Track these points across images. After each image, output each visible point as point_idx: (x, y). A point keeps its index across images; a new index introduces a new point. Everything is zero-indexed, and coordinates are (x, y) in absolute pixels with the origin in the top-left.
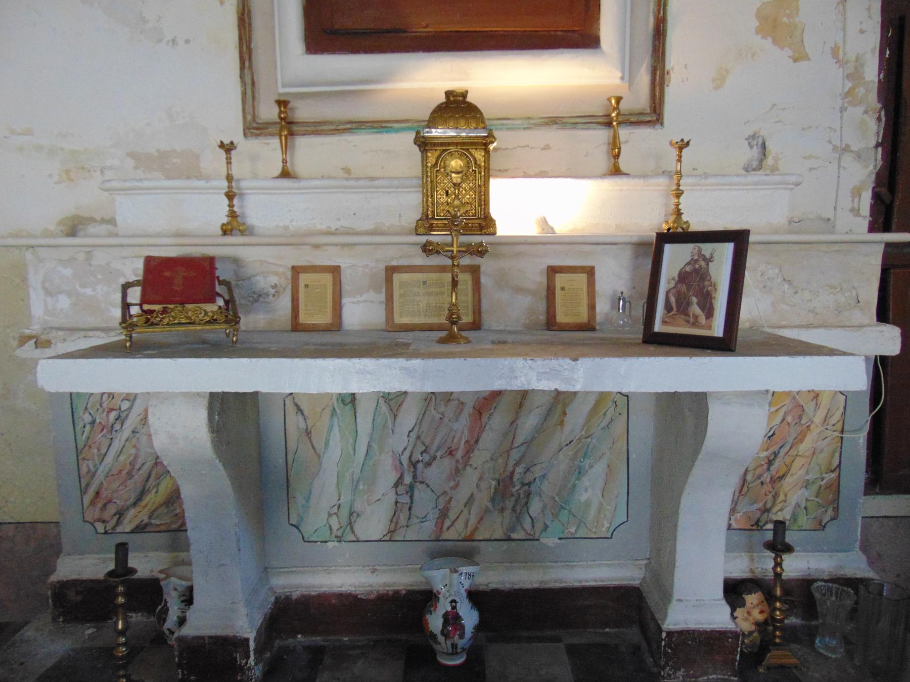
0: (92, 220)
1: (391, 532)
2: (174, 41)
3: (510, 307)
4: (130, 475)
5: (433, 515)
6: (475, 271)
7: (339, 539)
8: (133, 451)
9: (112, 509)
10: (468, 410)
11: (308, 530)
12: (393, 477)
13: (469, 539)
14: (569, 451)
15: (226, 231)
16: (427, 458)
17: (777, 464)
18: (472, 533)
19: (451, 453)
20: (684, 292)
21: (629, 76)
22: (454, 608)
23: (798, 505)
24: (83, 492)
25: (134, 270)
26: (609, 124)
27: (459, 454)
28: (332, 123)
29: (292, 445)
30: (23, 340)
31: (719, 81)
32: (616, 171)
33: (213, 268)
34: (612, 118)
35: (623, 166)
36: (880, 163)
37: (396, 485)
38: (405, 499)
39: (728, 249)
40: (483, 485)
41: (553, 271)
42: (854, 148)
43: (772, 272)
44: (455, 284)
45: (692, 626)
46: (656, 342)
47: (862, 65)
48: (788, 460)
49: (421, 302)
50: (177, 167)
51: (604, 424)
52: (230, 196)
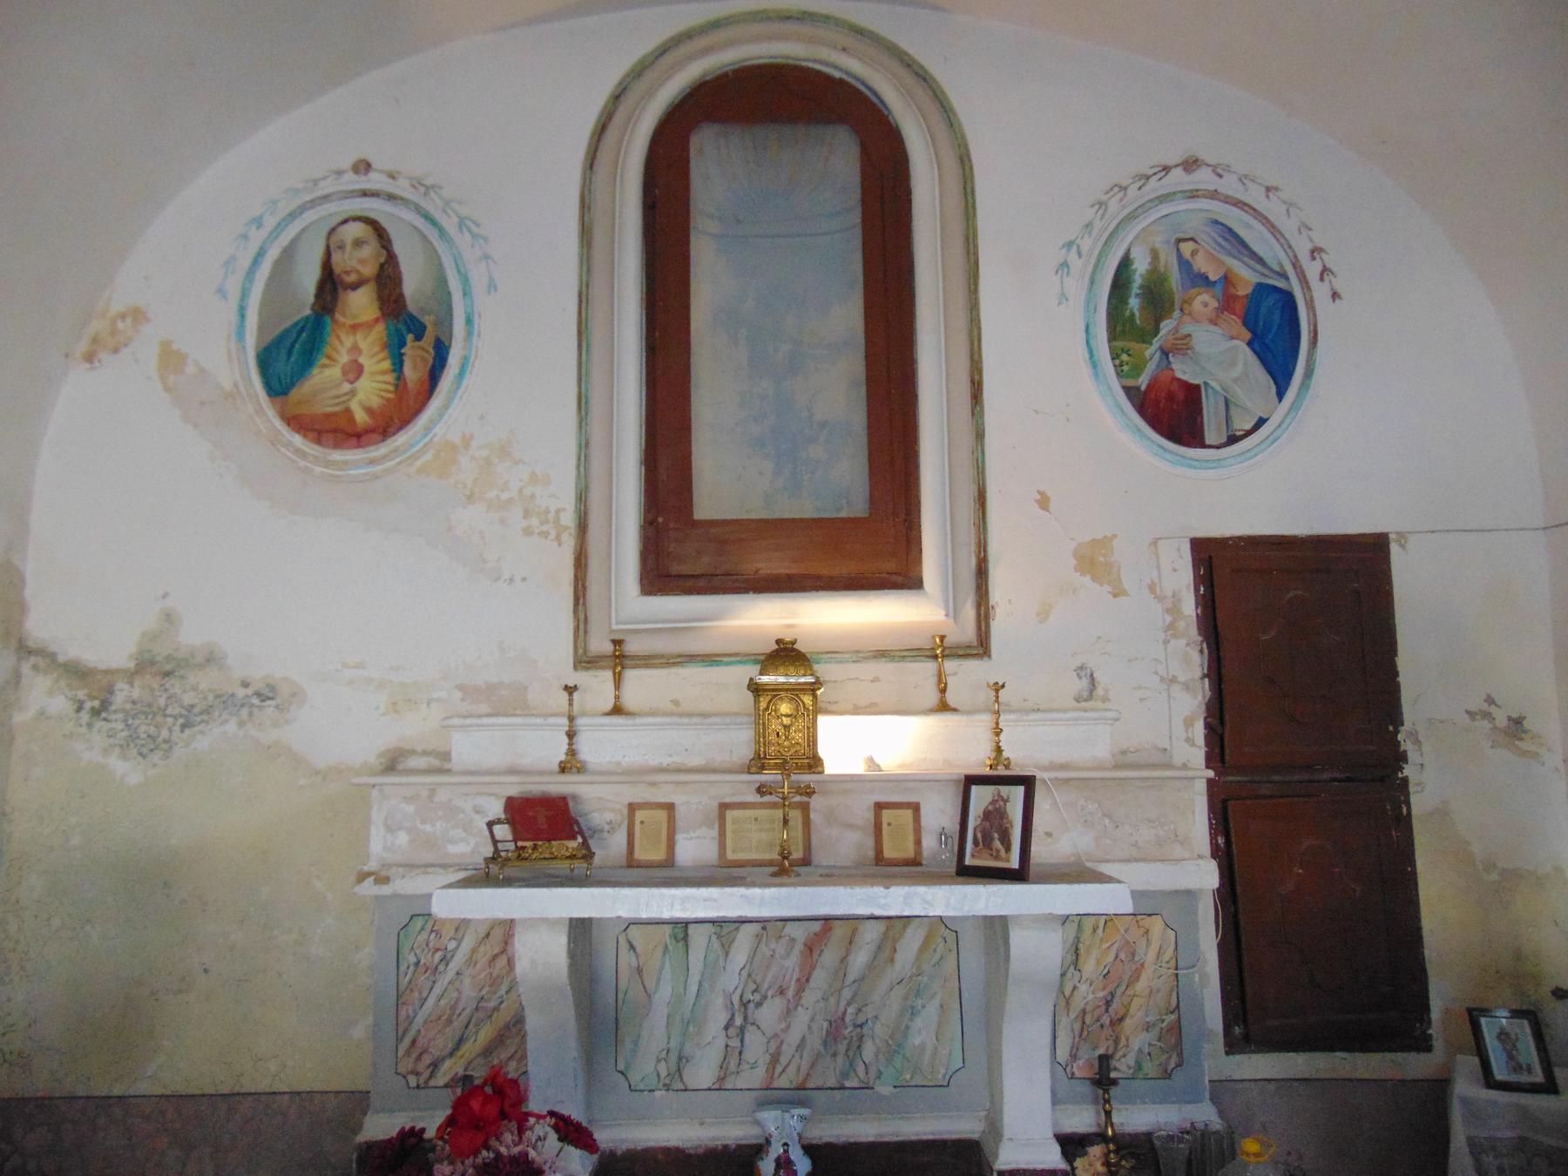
0: (413, 752)
1: (721, 1079)
2: (511, 580)
3: (843, 841)
4: (449, 1022)
5: (764, 1060)
6: (805, 808)
7: (667, 1087)
8: (455, 995)
9: (427, 1060)
10: (799, 947)
11: (635, 1077)
12: (723, 1018)
13: (801, 1088)
14: (900, 991)
15: (563, 769)
16: (757, 997)
17: (1114, 1005)
18: (805, 1080)
19: (782, 992)
20: (991, 828)
21: (954, 612)
22: (786, 1151)
23: (1140, 1051)
24: (399, 1040)
25: (496, 809)
26: (936, 657)
27: (790, 993)
28: (662, 656)
29: (623, 985)
30: (362, 877)
31: (1043, 615)
32: (944, 707)
33: (566, 804)
34: (939, 651)
35: (951, 698)
36: (1208, 694)
37: (726, 1028)
38: (735, 1043)
39: (1021, 789)
40: (815, 1026)
41: (879, 807)
42: (1182, 679)
43: (1092, 807)
44: (786, 822)
45: (1024, 1166)
46: (967, 873)
47: (1179, 600)
48: (1126, 1000)
49: (757, 835)
50: (504, 702)
51: (934, 961)
52: (571, 735)
